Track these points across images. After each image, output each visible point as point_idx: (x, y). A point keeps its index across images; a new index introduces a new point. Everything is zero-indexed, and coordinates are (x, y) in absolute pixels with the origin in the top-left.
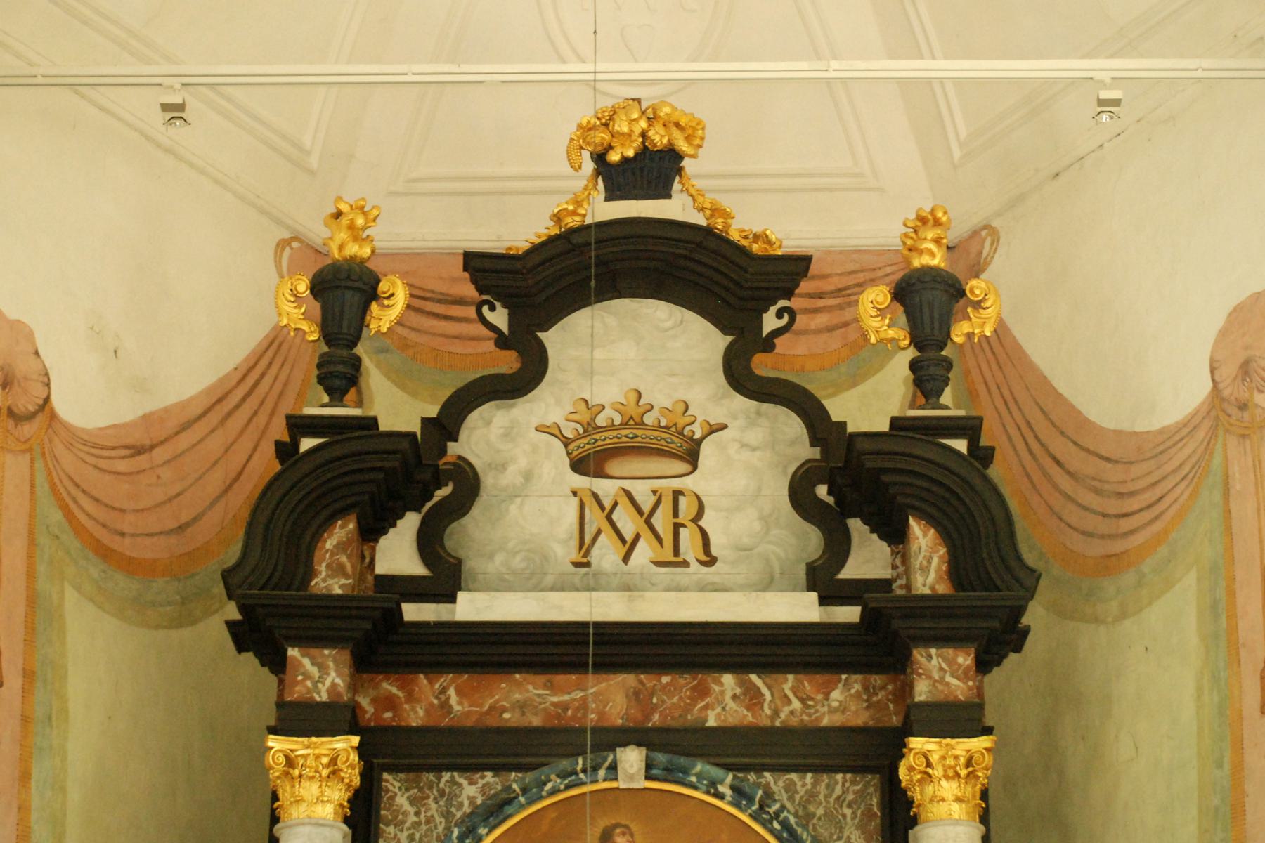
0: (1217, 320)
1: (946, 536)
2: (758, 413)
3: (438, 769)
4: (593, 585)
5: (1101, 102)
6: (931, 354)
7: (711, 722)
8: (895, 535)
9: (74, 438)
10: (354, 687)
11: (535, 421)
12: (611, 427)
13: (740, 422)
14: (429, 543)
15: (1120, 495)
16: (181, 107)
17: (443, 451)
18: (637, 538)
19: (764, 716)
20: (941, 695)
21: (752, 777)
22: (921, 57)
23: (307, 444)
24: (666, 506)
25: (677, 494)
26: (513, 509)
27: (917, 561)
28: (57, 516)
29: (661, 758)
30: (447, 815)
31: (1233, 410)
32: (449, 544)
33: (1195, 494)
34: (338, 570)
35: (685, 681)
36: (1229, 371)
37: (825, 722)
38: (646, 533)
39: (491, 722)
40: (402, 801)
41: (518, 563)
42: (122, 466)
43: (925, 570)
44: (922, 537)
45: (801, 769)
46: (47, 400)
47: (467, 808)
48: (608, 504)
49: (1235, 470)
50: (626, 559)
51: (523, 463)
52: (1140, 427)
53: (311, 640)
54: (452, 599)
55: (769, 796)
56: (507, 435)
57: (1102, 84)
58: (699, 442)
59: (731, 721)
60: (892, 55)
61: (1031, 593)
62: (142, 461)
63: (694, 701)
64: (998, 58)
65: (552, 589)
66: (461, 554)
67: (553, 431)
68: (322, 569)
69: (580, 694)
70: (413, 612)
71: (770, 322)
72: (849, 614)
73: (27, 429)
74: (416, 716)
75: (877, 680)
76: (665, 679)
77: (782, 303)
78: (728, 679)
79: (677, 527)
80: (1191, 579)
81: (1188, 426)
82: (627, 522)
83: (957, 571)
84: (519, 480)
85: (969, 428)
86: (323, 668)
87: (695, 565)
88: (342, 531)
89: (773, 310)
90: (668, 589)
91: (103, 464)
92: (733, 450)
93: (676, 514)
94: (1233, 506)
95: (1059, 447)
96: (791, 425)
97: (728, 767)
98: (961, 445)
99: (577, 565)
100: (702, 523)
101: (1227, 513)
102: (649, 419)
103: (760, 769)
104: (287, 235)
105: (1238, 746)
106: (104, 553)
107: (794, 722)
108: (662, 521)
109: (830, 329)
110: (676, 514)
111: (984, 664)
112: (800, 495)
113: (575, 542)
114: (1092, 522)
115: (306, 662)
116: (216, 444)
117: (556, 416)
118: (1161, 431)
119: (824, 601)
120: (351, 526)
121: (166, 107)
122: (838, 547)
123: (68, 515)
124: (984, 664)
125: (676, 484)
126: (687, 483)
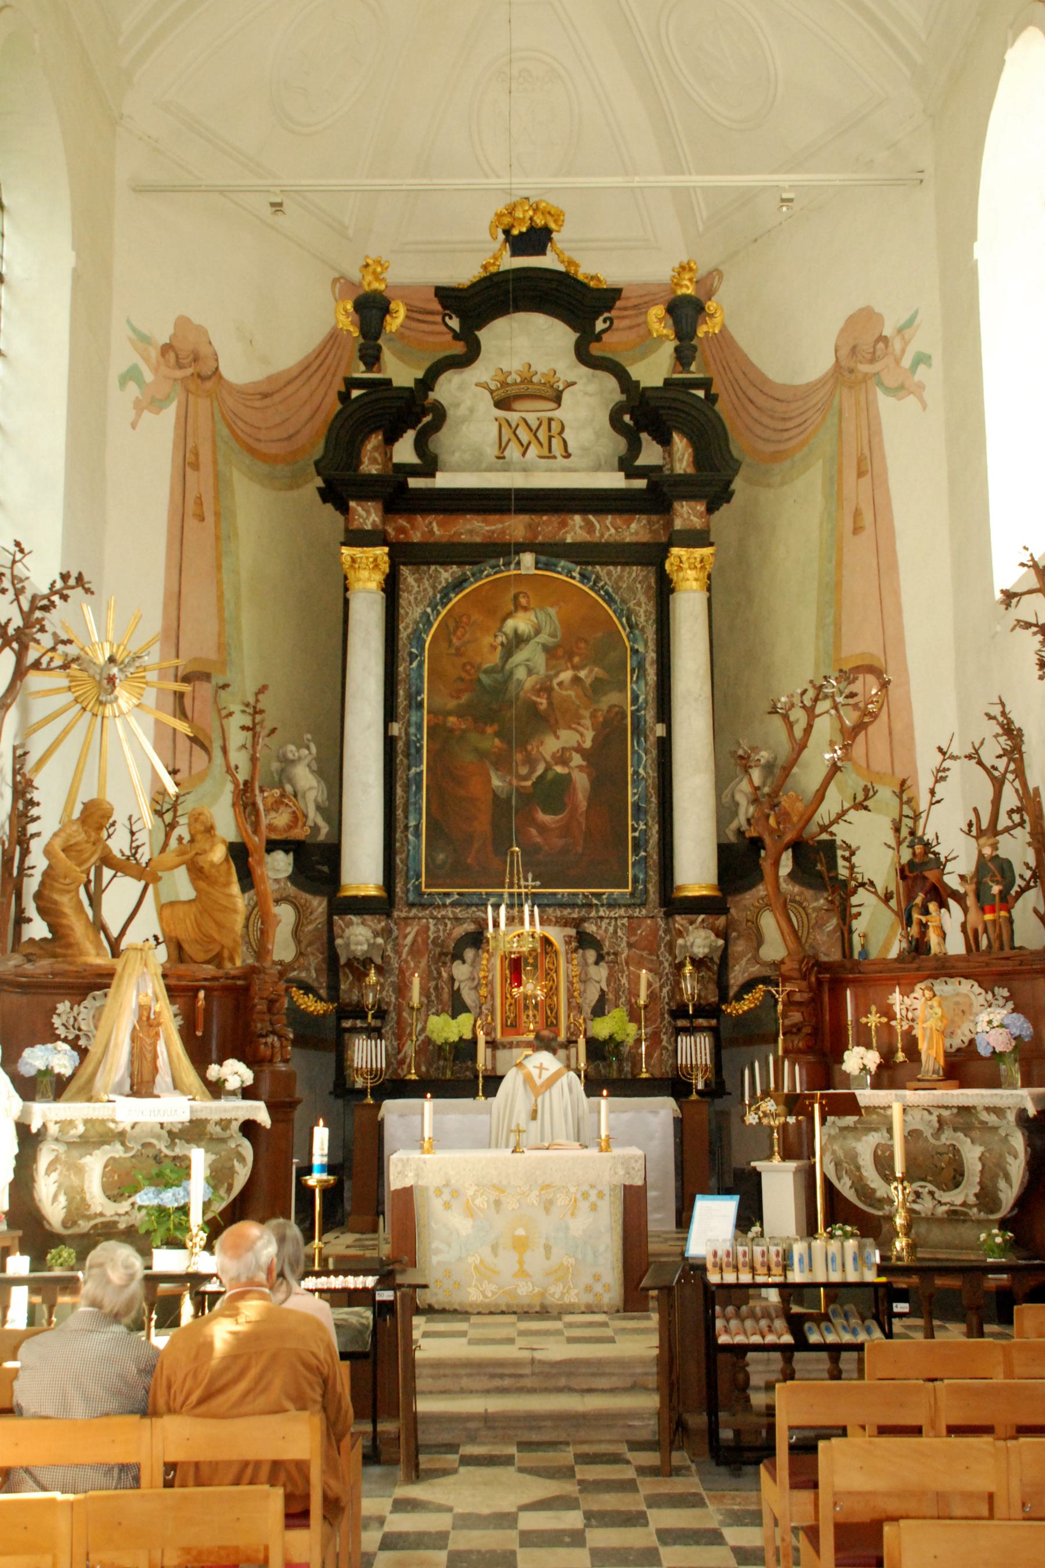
0: (841, 324)
2: (593, 376)
3: (429, 564)
5: (783, 200)
7: (569, 540)
8: (665, 441)
10: (384, 522)
11: (475, 380)
12: (516, 383)
13: (584, 380)
14: (421, 446)
15: (784, 419)
16: (280, 205)
17: (426, 396)
18: (529, 444)
21: (590, 568)
22: (683, 173)
23: (355, 393)
24: (545, 426)
25: (550, 420)
27: (677, 455)
29: (543, 558)
30: (434, 587)
31: (846, 373)
34: (373, 461)
36: (844, 352)
37: (628, 540)
38: (534, 441)
39: (455, 540)
40: (411, 580)
41: (467, 456)
42: (258, 404)
43: (681, 460)
44: (680, 443)
45: (615, 564)
46: (217, 369)
47: (444, 584)
48: (514, 426)
50: (524, 454)
51: (469, 403)
53: (361, 498)
54: (433, 476)
55: (598, 578)
57: (784, 190)
58: (561, 392)
59: (579, 539)
60: (668, 173)
61: (736, 472)
62: (267, 402)
63: (560, 529)
65: (486, 470)
66: (437, 452)
67: (485, 386)
68: (366, 460)
69: (500, 526)
70: (414, 483)
71: (600, 325)
72: (641, 484)
73: (209, 385)
74: (416, 537)
75: (654, 518)
76: (545, 518)
77: (606, 315)
78: (577, 518)
79: (550, 438)
80: (820, 463)
81: (822, 382)
82: (524, 435)
83: (699, 460)
84: (467, 413)
85: (705, 384)
86: (368, 512)
87: (560, 458)
88: (375, 440)
89: (601, 318)
90: (546, 471)
91: (248, 403)
93: (550, 430)
94: (843, 425)
95: (752, 393)
96: (611, 383)
97: (578, 563)
98: (701, 393)
99: (498, 458)
100: (564, 435)
102: (535, 379)
103: (593, 564)
104: (337, 276)
105: (840, 550)
106: (252, 451)
107: (612, 540)
108: (542, 434)
109: (630, 328)
110: (550, 430)
111: (710, 510)
113: (497, 446)
115: (359, 509)
118: (808, 384)
119: (628, 476)
120: (380, 437)
121: (273, 205)
122: (635, 447)
123: (233, 432)
124: (710, 510)
125: (550, 414)
126: (557, 414)
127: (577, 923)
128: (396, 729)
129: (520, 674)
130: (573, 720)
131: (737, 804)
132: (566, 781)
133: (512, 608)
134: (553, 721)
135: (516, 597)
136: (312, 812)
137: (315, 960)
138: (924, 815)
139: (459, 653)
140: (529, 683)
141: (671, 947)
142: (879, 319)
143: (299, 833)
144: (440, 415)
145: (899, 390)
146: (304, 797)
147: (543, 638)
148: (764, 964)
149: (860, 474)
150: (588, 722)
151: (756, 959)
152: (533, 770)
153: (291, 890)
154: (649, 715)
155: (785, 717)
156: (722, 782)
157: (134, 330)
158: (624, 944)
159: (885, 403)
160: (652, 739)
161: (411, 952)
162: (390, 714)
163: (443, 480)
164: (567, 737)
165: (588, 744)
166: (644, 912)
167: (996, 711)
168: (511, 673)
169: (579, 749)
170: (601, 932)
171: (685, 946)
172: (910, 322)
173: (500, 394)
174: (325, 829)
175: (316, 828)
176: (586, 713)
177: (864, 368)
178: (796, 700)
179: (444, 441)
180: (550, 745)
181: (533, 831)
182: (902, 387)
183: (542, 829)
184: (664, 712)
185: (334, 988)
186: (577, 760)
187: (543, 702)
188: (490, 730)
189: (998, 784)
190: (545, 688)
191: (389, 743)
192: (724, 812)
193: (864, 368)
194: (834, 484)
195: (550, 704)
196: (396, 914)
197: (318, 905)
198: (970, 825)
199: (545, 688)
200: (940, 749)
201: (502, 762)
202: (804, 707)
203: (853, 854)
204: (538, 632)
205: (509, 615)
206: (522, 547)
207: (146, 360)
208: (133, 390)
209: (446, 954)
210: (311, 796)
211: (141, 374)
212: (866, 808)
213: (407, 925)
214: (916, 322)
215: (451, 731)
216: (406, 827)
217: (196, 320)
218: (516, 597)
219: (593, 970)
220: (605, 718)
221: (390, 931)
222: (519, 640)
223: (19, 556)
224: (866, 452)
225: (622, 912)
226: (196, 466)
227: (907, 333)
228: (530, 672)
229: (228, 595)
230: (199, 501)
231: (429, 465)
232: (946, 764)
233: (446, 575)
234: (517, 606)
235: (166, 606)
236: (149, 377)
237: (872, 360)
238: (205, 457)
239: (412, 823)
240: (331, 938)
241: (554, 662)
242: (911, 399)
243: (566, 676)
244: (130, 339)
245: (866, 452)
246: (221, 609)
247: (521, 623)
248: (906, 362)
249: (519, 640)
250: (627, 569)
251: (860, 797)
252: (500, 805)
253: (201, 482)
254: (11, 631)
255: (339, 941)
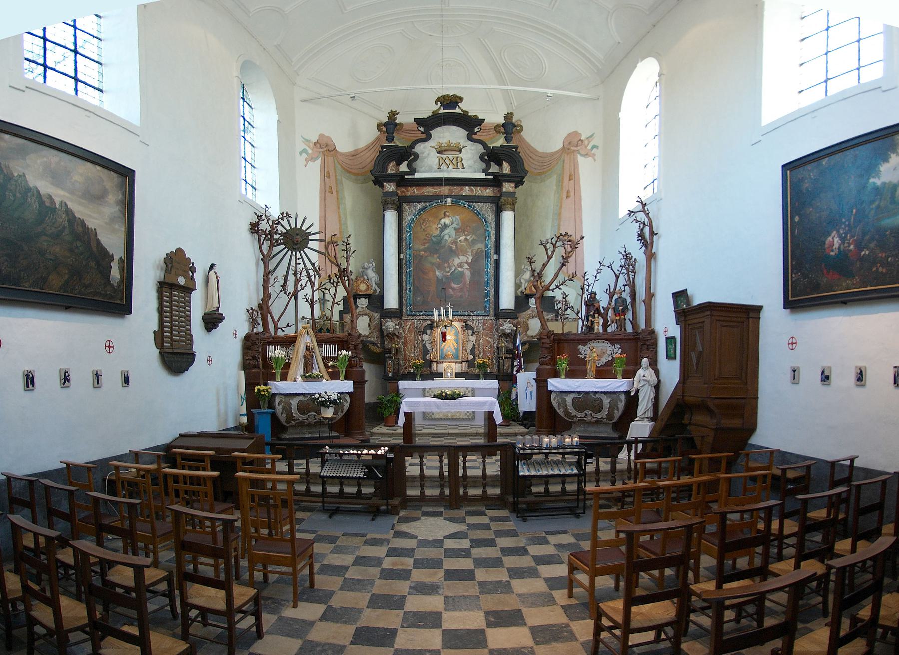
1: (510, 164)
4: (442, 171)
6: (509, 135)
8: (500, 164)
9: (341, 154)
10: (396, 189)
14: (409, 166)
19: (474, 194)
20: (508, 190)
24: (455, 159)
26: (426, 160)
28: (339, 166)
32: (413, 166)
33: (558, 163)
35: (459, 187)
36: (567, 143)
40: (406, 207)
42: (351, 158)
43: (506, 170)
44: (505, 164)
49: (566, 159)
51: (427, 152)
52: (548, 152)
53: (387, 181)
54: (414, 174)
56: (424, 148)
60: (500, 85)
61: (526, 174)
64: (524, 87)
67: (433, 147)
68: (389, 170)
70: (406, 177)
71: (476, 130)
73: (332, 153)
74: (408, 194)
75: (496, 188)
78: (467, 187)
80: (555, 176)
82: (448, 162)
83: (512, 170)
85: (516, 147)
86: (390, 186)
88: (393, 163)
92: (469, 150)
94: (565, 164)
95: (531, 155)
101: (563, 166)
103: (473, 202)
106: (349, 172)
111: (516, 187)
112: (482, 157)
114: (536, 167)
116: (368, 154)
117: (433, 144)
122: (489, 166)
123: (341, 165)
124: (516, 187)
125: (457, 155)
127: (466, 321)
128: (402, 256)
129: (446, 237)
130: (465, 253)
131: (522, 283)
132: (462, 274)
133: (443, 216)
134: (458, 253)
135: (445, 213)
136: (374, 285)
137: (376, 334)
138: (592, 285)
139: (424, 231)
140: (449, 241)
141: (497, 330)
142: (580, 135)
143: (369, 292)
144: (416, 156)
145: (586, 155)
146: (371, 280)
147: (454, 226)
148: (529, 337)
149: (570, 180)
150: (470, 254)
151: (526, 335)
152: (450, 270)
153: (367, 311)
154: (492, 252)
155: (545, 247)
156: (518, 273)
157: (303, 138)
158: (482, 329)
159: (581, 159)
160: (493, 260)
161: (408, 331)
162: (400, 251)
163: (417, 175)
164: (463, 259)
165: (470, 261)
166: (489, 318)
167: (622, 251)
168: (443, 237)
169: (467, 263)
170: (474, 324)
171: (503, 330)
172: (591, 136)
173: (439, 149)
174: (378, 290)
175: (375, 291)
176: (470, 251)
177: (573, 148)
178: (550, 241)
179: (417, 164)
180: (457, 261)
181: (451, 290)
182: (587, 154)
183: (454, 289)
184: (498, 250)
185: (382, 343)
186: (466, 266)
187: (454, 247)
188: (435, 256)
189: (617, 277)
190: (455, 242)
191: (400, 261)
192: (517, 286)
193: (573, 148)
194: (560, 182)
195: (457, 247)
196: (403, 318)
197: (377, 316)
198: (607, 290)
199: (455, 242)
200: (600, 262)
201: (439, 267)
202: (552, 244)
203: (567, 296)
204: (452, 224)
205: (442, 218)
206: (446, 196)
207: (309, 147)
208: (304, 155)
209: (420, 332)
210: (373, 280)
211: (307, 150)
212: (573, 280)
213: (407, 322)
214: (595, 135)
215: (422, 256)
216: (406, 289)
217: (326, 134)
218: (445, 213)
219: (471, 337)
220: (476, 253)
221: (401, 324)
222: (445, 226)
223: (267, 209)
224: (573, 173)
225: (481, 318)
226: (329, 177)
227: (590, 139)
228: (450, 237)
229: (342, 215)
230: (331, 187)
231: (413, 171)
232: (601, 268)
233: (419, 206)
234: (445, 215)
235: (320, 193)
236: (310, 151)
237: (577, 146)
238: (332, 173)
239: (408, 288)
240: (381, 326)
241: (458, 234)
242: (590, 158)
243: (463, 238)
244: (303, 142)
245: (573, 173)
246: (340, 221)
247: (447, 221)
248: (589, 147)
249: (445, 226)
250: (485, 204)
251: (571, 277)
252: (439, 281)
253: (331, 182)
254: (267, 232)
255: (384, 327)
